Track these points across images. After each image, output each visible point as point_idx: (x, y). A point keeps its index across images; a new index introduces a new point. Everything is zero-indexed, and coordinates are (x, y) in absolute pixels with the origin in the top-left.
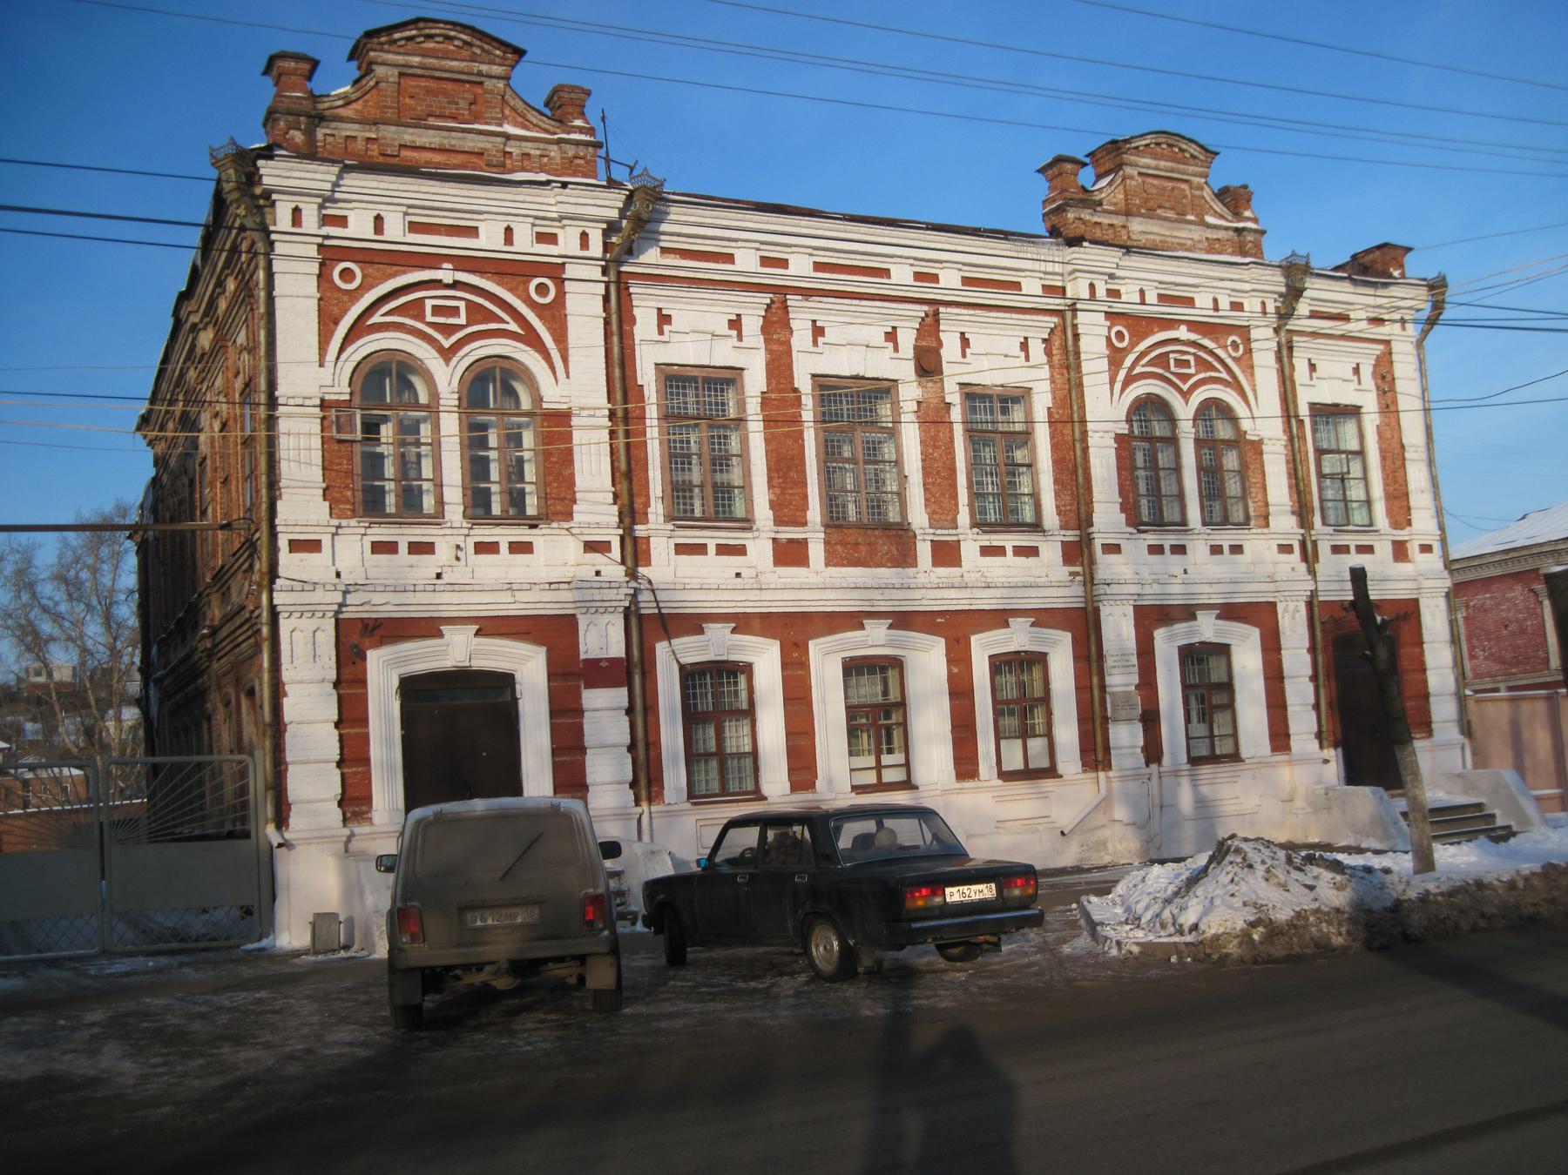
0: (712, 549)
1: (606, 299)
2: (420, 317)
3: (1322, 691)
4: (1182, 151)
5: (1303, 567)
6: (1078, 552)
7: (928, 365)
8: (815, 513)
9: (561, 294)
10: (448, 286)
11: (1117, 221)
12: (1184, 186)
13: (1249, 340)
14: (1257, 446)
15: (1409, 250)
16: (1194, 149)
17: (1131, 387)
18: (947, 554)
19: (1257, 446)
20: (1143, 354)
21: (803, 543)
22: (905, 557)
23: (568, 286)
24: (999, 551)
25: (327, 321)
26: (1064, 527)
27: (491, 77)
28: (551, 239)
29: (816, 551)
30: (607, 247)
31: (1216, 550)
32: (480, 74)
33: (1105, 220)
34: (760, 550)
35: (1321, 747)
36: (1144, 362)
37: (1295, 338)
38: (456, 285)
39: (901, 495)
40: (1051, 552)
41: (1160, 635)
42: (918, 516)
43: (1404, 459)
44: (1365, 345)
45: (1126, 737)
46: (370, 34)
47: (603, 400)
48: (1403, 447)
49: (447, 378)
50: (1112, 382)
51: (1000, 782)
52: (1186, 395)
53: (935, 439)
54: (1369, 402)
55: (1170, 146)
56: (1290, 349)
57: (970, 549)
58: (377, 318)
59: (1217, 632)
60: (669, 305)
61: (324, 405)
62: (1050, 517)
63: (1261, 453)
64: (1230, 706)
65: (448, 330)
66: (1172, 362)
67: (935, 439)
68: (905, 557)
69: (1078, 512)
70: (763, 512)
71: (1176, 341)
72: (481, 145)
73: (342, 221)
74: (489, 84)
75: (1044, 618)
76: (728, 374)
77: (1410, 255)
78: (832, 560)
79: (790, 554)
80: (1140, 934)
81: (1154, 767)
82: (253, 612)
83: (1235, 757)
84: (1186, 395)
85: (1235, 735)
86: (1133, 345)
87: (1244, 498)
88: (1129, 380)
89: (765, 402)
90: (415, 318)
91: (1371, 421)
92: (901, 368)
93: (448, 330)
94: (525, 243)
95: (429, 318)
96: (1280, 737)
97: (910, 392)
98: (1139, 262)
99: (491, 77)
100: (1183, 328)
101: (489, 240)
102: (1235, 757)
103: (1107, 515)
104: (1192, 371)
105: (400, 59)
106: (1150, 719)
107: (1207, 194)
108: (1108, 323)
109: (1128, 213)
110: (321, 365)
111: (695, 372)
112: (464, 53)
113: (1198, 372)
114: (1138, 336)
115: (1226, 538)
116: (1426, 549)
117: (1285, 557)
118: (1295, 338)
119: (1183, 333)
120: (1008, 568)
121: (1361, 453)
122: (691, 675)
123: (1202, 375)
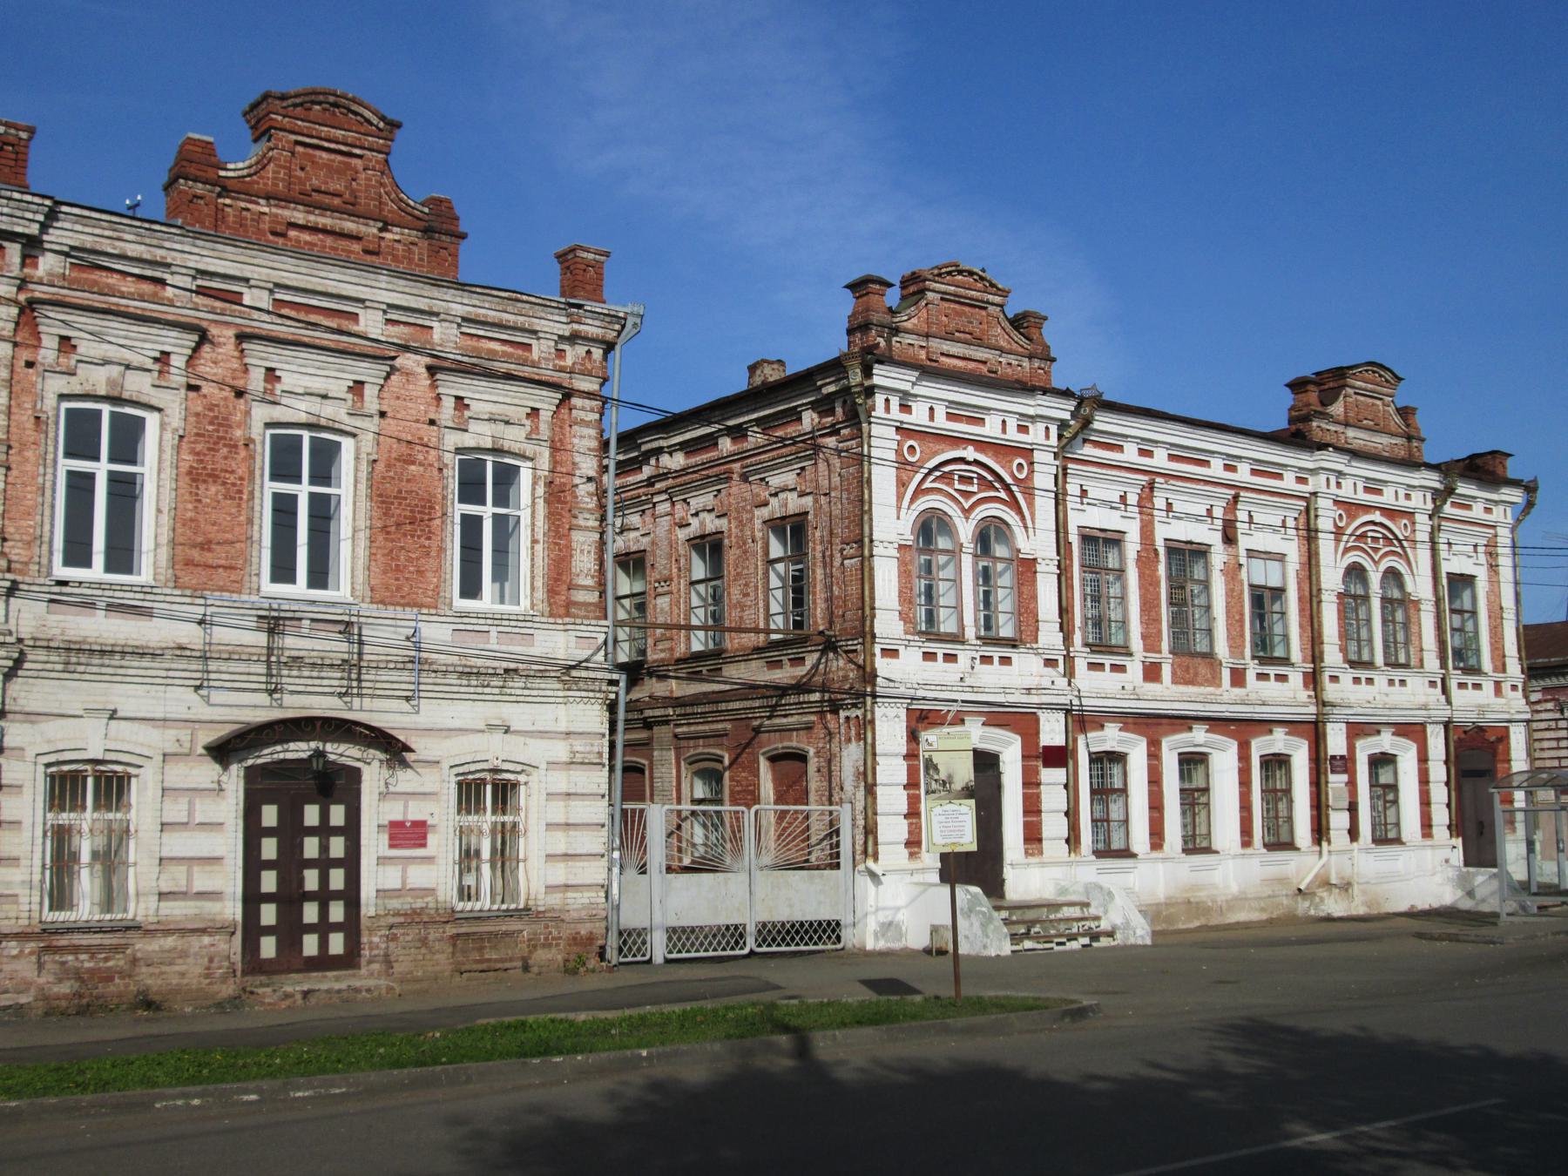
0: (1107, 667)
1: (1056, 476)
2: (950, 484)
3: (1453, 794)
4: (1380, 376)
5: (1443, 698)
6: (1313, 679)
7: (1229, 539)
8: (1165, 645)
9: (1031, 472)
10: (968, 463)
11: (1340, 428)
12: (1379, 402)
13: (1414, 523)
14: (1417, 603)
15: (1510, 455)
16: (1388, 376)
17: (918, 502)
18: (1238, 678)
19: (1417, 603)
20: (931, 471)
21: (87, 563)
22: (1215, 680)
23: (1036, 467)
24: (1100, 666)
25: (902, 484)
26: (1304, 661)
27: (993, 304)
28: (1149, 454)
29: (1166, 671)
30: (1060, 437)
31: (1357, 680)
32: (988, 302)
33: (1332, 428)
34: (1135, 668)
35: (1451, 836)
36: (932, 478)
37: (1070, 466)
38: (977, 463)
39: (1209, 632)
40: (1296, 678)
41: (1359, 744)
42: (1222, 649)
43: (1502, 618)
44: (1114, 472)
45: (1338, 821)
46: (266, 96)
47: (1053, 554)
48: (1501, 608)
49: (966, 530)
50: (1336, 551)
51: (1265, 851)
52: (967, 512)
53: (1232, 590)
54: (1482, 574)
55: (1374, 372)
56: (1065, 475)
57: (1250, 676)
58: (927, 485)
59: (1392, 745)
60: (470, 395)
61: (901, 547)
62: (1296, 655)
63: (1419, 610)
64: (1395, 802)
65: (966, 494)
66: (956, 477)
67: (1232, 590)
68: (1215, 680)
69: (1315, 655)
70: (1136, 644)
71: (962, 460)
72: (986, 356)
73: (910, 412)
74: (991, 308)
75: (1293, 726)
76: (1116, 536)
77: (1510, 459)
78: (1174, 682)
79: (1152, 673)
80: (177, 968)
81: (1355, 844)
82: (417, 661)
83: (1398, 841)
84: (967, 512)
85: (1398, 825)
86: (1348, 524)
87: (1407, 643)
88: (919, 492)
89: (1139, 559)
90: (948, 484)
91: (1482, 586)
92: (1214, 538)
93: (966, 494)
94: (1013, 434)
95: (957, 486)
96: (1427, 826)
97: (1219, 556)
98: (287, 278)
99: (993, 304)
100: (1378, 513)
101: (991, 429)
102: (1398, 841)
103: (1332, 655)
104: (974, 488)
105: (943, 287)
106: (1353, 809)
107: (1391, 409)
108: (898, 438)
109: (1347, 425)
110: (898, 518)
111: (1182, 546)
112: (980, 285)
113: (980, 491)
114: (1352, 518)
115: (1397, 674)
116: (1514, 688)
117: (1432, 690)
118: (1070, 466)
119: (1377, 517)
120: (1271, 689)
121: (1474, 613)
122: (1097, 759)
123: (1387, 549)
